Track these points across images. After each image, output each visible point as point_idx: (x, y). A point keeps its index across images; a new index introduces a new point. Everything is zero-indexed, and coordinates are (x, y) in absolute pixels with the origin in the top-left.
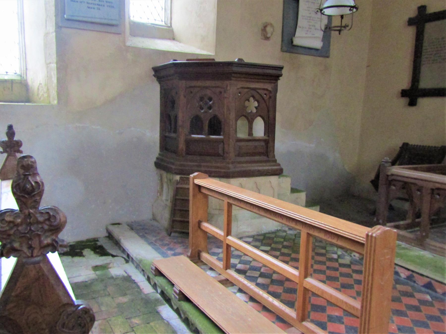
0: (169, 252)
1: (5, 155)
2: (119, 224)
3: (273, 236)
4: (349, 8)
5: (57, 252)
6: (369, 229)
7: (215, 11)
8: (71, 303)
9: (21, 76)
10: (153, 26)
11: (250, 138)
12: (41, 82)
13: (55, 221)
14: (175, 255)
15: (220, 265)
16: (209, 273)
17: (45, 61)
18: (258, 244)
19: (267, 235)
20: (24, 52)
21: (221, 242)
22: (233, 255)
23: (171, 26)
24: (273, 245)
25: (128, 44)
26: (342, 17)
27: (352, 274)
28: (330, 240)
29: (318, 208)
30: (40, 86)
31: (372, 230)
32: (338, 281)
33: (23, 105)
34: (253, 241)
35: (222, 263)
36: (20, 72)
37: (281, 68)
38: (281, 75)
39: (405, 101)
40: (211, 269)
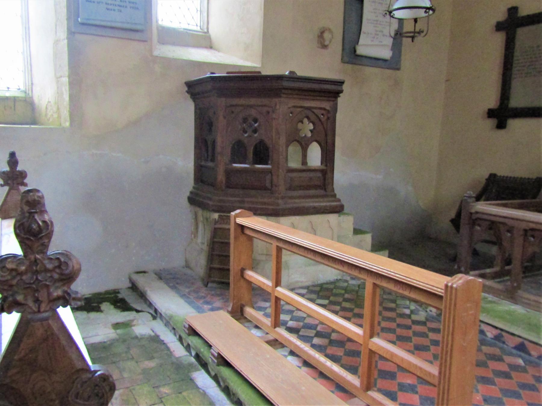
0: (205, 306)
1: (7, 188)
2: (144, 272)
3: (332, 286)
4: (425, 10)
5: (69, 307)
6: (449, 278)
7: (262, 13)
8: (87, 369)
9: (25, 92)
10: (187, 32)
11: (304, 168)
12: (50, 100)
13: (67, 269)
14: (212, 310)
15: (268, 322)
16: (254, 331)
17: (55, 74)
18: (314, 296)
19: (325, 286)
20: (29, 64)
21: (269, 294)
22: (283, 310)
23: (208, 31)
24: (332, 298)
25: (156, 53)
26: (416, 20)
27: (428, 333)
28: (401, 291)
29: (387, 252)
30: (49, 104)
31: (452, 280)
32: (411, 342)
33: (28, 127)
34: (307, 293)
35: (270, 319)
36: (25, 88)
37: (342, 83)
38: (341, 92)
39: (492, 122)
40: (257, 327)
